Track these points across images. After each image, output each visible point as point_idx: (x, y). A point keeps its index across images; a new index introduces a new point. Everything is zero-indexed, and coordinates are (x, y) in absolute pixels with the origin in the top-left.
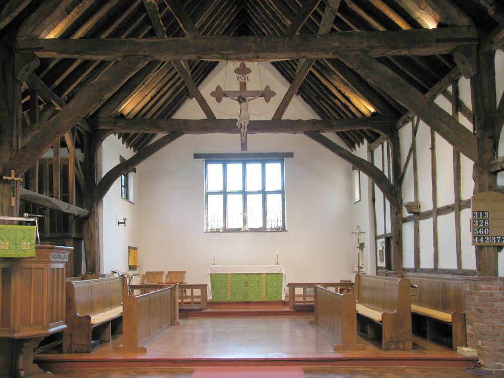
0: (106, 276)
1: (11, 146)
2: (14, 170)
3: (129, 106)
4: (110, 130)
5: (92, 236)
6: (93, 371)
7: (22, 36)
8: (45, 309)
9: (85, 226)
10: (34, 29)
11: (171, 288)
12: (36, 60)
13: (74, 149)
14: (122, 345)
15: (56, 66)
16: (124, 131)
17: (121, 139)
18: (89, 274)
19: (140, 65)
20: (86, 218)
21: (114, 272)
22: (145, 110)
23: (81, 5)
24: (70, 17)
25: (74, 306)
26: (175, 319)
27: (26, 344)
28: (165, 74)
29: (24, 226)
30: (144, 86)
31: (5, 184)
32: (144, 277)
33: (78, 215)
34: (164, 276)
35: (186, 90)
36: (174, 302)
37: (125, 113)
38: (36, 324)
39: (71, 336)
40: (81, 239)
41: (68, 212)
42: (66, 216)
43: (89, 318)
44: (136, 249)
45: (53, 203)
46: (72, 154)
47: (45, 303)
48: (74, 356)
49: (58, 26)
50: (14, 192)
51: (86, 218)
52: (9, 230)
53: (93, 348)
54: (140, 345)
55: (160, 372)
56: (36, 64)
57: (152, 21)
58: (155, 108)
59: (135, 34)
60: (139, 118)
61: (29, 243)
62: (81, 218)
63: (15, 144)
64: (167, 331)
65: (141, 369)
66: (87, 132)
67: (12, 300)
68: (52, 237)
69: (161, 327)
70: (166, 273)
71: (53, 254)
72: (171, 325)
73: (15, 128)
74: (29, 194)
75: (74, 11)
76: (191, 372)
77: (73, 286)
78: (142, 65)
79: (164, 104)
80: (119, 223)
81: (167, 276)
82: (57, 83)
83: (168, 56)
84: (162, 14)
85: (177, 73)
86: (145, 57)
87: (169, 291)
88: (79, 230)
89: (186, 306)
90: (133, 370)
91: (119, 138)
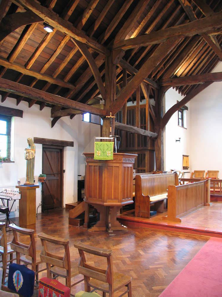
0: (167, 172)
1: (110, 99)
2: (111, 112)
3: (180, 70)
4: (169, 86)
5: (159, 149)
6: (148, 230)
7: (116, 42)
8: (120, 192)
9: (156, 143)
10: (122, 36)
11: (205, 182)
12: (123, 52)
13: (148, 99)
14: (167, 216)
15: (136, 54)
16: (180, 85)
17: (178, 91)
18: (157, 171)
19: (176, 41)
20: (156, 138)
21: (172, 170)
22: (191, 72)
23: (146, 18)
24: (140, 26)
25: (141, 190)
26: (207, 202)
27: (111, 210)
28: (201, 48)
29: (103, 142)
30: (188, 57)
31: (107, 121)
32: (192, 174)
33: (151, 137)
34: (205, 174)
35: (217, 56)
36: (207, 191)
37: (179, 75)
38: (115, 198)
39: (139, 207)
40: (154, 151)
41: (145, 134)
42: (145, 137)
43: (148, 197)
44: (187, 156)
45: (135, 130)
46: (147, 102)
47: (120, 187)
48: (140, 220)
49: (135, 32)
50: (111, 124)
51: (156, 138)
52: (101, 145)
53: (151, 215)
54: (177, 217)
55: (186, 236)
56: (123, 54)
57: (189, 17)
58: (197, 70)
59: (172, 24)
60: (188, 76)
61: (110, 152)
62: (153, 138)
63: (112, 98)
64: (200, 209)
65: (177, 233)
66: (156, 89)
67: (103, 184)
68: (139, 149)
69: (196, 206)
70: (206, 171)
71: (124, 158)
72: (204, 206)
73: (112, 90)
74: (121, 125)
75: (143, 22)
76: (206, 240)
77: (140, 178)
78: (178, 41)
79: (203, 66)
80: (176, 141)
81: (207, 174)
82: (137, 63)
83: (193, 32)
84: (196, 11)
85: (209, 47)
86: (179, 36)
87: (203, 183)
88: (153, 145)
89: (217, 193)
90: (171, 233)
91: (176, 90)
